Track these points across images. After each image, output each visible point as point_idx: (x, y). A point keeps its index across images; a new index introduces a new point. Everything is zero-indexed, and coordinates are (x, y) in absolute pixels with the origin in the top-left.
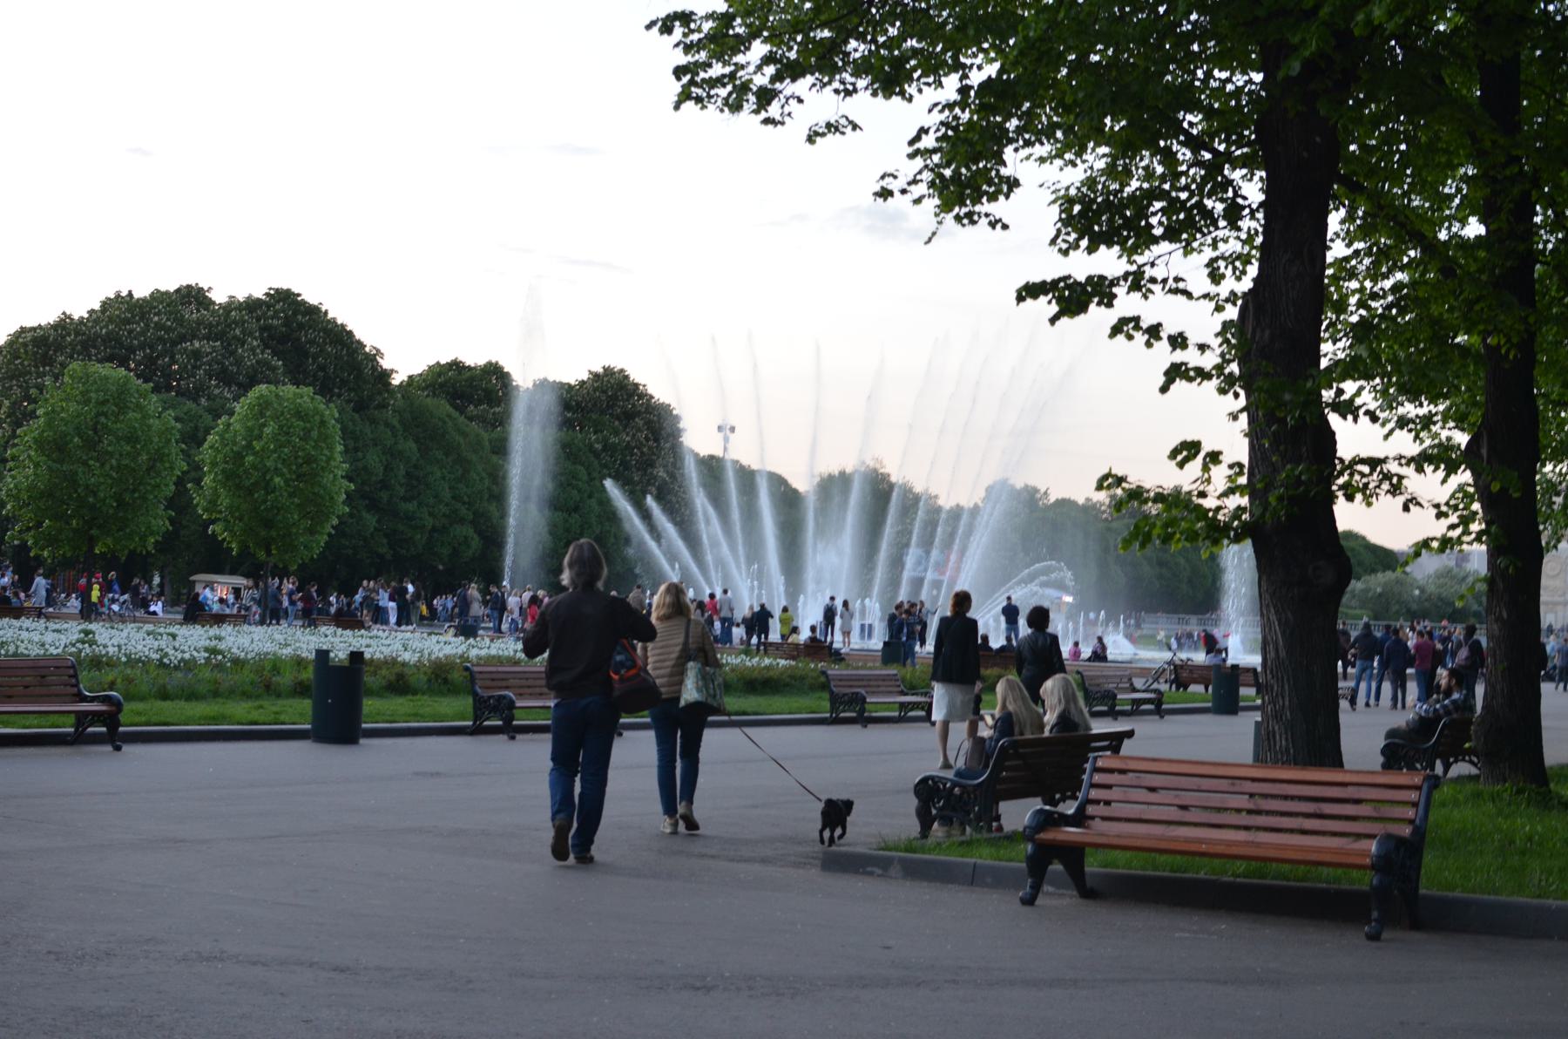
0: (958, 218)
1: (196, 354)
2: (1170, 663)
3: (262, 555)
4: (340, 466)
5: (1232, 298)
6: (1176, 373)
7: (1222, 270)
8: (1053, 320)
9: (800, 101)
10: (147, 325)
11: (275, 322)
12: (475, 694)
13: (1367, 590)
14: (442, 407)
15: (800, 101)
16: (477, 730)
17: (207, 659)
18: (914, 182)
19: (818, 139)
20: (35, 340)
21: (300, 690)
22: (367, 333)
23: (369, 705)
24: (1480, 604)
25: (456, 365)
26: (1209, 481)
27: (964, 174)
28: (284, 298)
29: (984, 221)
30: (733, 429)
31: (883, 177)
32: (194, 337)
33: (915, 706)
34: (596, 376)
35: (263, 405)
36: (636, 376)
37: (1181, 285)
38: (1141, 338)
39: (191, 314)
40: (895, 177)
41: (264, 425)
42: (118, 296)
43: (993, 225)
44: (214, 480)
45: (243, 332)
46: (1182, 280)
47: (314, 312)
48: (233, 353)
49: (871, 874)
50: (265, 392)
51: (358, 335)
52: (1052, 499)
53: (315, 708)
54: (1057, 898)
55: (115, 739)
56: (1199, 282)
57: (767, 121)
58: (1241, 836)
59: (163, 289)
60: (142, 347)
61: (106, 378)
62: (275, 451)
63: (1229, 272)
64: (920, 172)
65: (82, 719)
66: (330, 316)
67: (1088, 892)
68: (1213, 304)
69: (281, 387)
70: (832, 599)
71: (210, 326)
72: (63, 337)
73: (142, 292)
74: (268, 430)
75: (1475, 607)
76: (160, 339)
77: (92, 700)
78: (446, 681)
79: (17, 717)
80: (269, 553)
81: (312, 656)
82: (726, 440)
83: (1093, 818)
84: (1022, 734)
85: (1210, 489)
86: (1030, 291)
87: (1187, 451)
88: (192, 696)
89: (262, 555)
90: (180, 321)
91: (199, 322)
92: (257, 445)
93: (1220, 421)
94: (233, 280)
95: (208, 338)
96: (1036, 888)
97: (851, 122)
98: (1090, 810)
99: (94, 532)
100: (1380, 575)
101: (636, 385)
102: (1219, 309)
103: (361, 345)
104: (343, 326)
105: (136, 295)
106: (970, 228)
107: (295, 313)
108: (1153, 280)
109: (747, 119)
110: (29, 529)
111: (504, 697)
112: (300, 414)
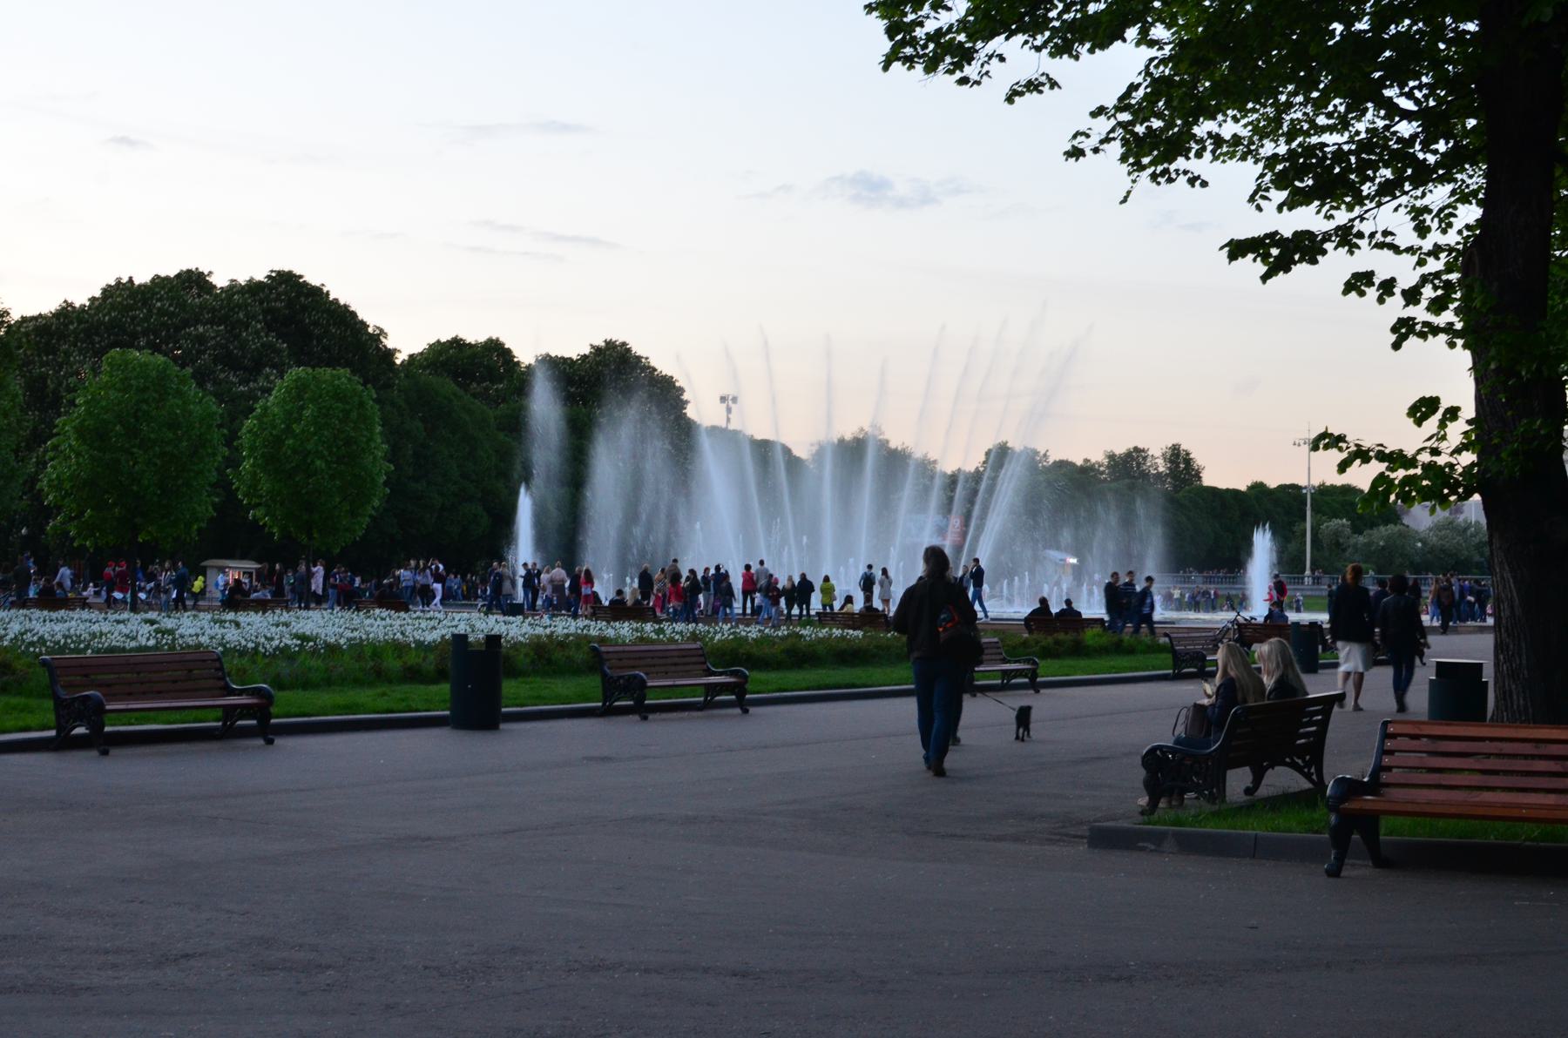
0: (1154, 177)
1: (201, 339)
2: (1235, 622)
3: (304, 539)
4: (381, 447)
5: (1436, 251)
6: (1403, 329)
7: (1428, 222)
8: (1265, 278)
9: (1002, 59)
10: (150, 311)
11: (278, 304)
12: (604, 675)
13: (1368, 545)
14: (447, 386)
15: (1002, 59)
16: (607, 712)
17: (301, 646)
18: (1107, 140)
19: (1016, 98)
20: (36, 329)
21: (440, 675)
22: (370, 315)
23: (509, 687)
24: (1482, 555)
25: (456, 343)
26: (1444, 438)
27: (1155, 136)
28: (286, 282)
29: (1183, 179)
30: (735, 400)
31: (1075, 137)
32: (197, 322)
33: (1019, 673)
34: (597, 351)
35: (300, 388)
36: (638, 348)
37: (1389, 239)
38: (1372, 293)
39: (193, 299)
40: (1088, 136)
41: (302, 408)
42: (119, 282)
43: (1192, 182)
44: (253, 466)
45: (246, 315)
46: (1392, 234)
47: (317, 293)
48: (237, 337)
49: (1143, 849)
50: (303, 375)
51: (361, 316)
52: (1051, 460)
53: (453, 691)
54: (1357, 869)
55: (267, 732)
56: (1406, 235)
57: (964, 81)
58: (1551, 799)
59: (163, 275)
60: (145, 333)
61: (146, 365)
62: (315, 434)
63: (1435, 225)
64: (1113, 130)
65: (230, 713)
66: (331, 297)
67: (1383, 860)
68: (1415, 258)
69: (318, 370)
70: (870, 567)
71: (213, 310)
72: (66, 326)
73: (142, 278)
74: (307, 413)
75: (1477, 558)
76: (164, 324)
77: (240, 693)
78: (549, 661)
79: (152, 714)
80: (310, 538)
81: (1106, 462)
82: (729, 410)
83: (1388, 785)
84: (1245, 701)
85: (1443, 445)
86: (1237, 249)
87: (1423, 409)
88: (328, 682)
89: (304, 539)
90: (182, 305)
91: (202, 307)
92: (297, 428)
93: (1450, 373)
94: (233, 264)
95: (212, 322)
96: (1340, 860)
97: (1050, 80)
98: (1384, 777)
99: (138, 520)
100: (1382, 528)
101: (639, 358)
102: (1421, 263)
103: (364, 325)
104: (346, 306)
105: (137, 282)
106: (1164, 187)
107: (298, 297)
108: (1360, 235)
109: (943, 81)
110: (72, 519)
111: (635, 676)
112: (339, 395)
